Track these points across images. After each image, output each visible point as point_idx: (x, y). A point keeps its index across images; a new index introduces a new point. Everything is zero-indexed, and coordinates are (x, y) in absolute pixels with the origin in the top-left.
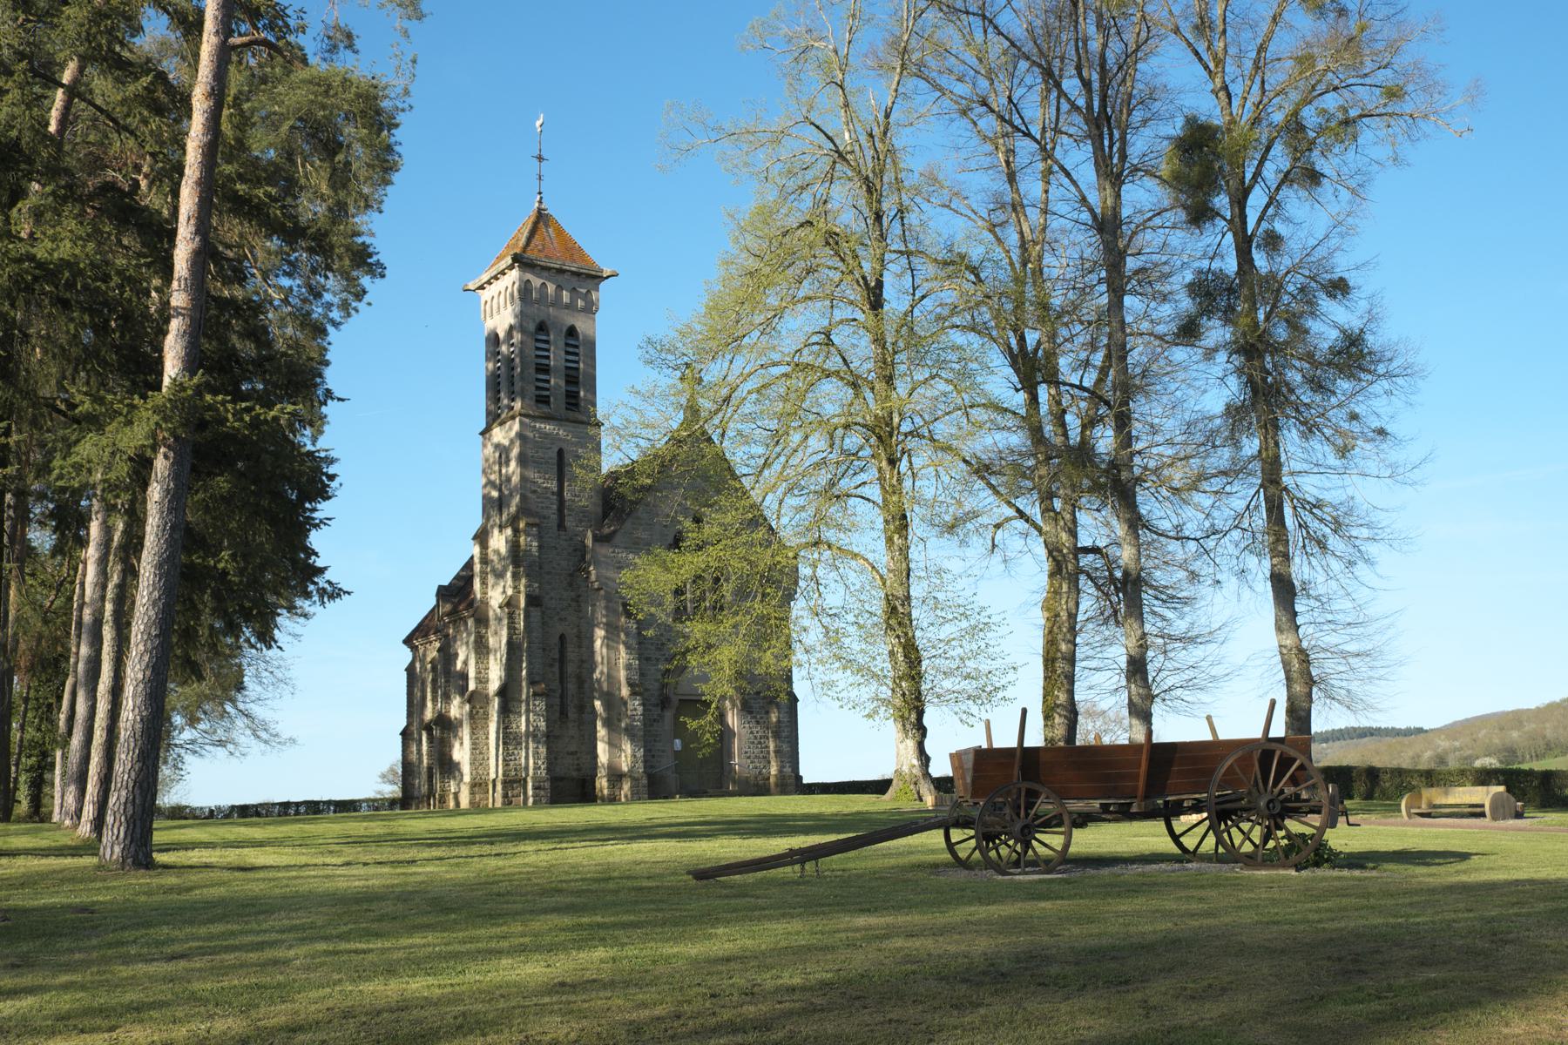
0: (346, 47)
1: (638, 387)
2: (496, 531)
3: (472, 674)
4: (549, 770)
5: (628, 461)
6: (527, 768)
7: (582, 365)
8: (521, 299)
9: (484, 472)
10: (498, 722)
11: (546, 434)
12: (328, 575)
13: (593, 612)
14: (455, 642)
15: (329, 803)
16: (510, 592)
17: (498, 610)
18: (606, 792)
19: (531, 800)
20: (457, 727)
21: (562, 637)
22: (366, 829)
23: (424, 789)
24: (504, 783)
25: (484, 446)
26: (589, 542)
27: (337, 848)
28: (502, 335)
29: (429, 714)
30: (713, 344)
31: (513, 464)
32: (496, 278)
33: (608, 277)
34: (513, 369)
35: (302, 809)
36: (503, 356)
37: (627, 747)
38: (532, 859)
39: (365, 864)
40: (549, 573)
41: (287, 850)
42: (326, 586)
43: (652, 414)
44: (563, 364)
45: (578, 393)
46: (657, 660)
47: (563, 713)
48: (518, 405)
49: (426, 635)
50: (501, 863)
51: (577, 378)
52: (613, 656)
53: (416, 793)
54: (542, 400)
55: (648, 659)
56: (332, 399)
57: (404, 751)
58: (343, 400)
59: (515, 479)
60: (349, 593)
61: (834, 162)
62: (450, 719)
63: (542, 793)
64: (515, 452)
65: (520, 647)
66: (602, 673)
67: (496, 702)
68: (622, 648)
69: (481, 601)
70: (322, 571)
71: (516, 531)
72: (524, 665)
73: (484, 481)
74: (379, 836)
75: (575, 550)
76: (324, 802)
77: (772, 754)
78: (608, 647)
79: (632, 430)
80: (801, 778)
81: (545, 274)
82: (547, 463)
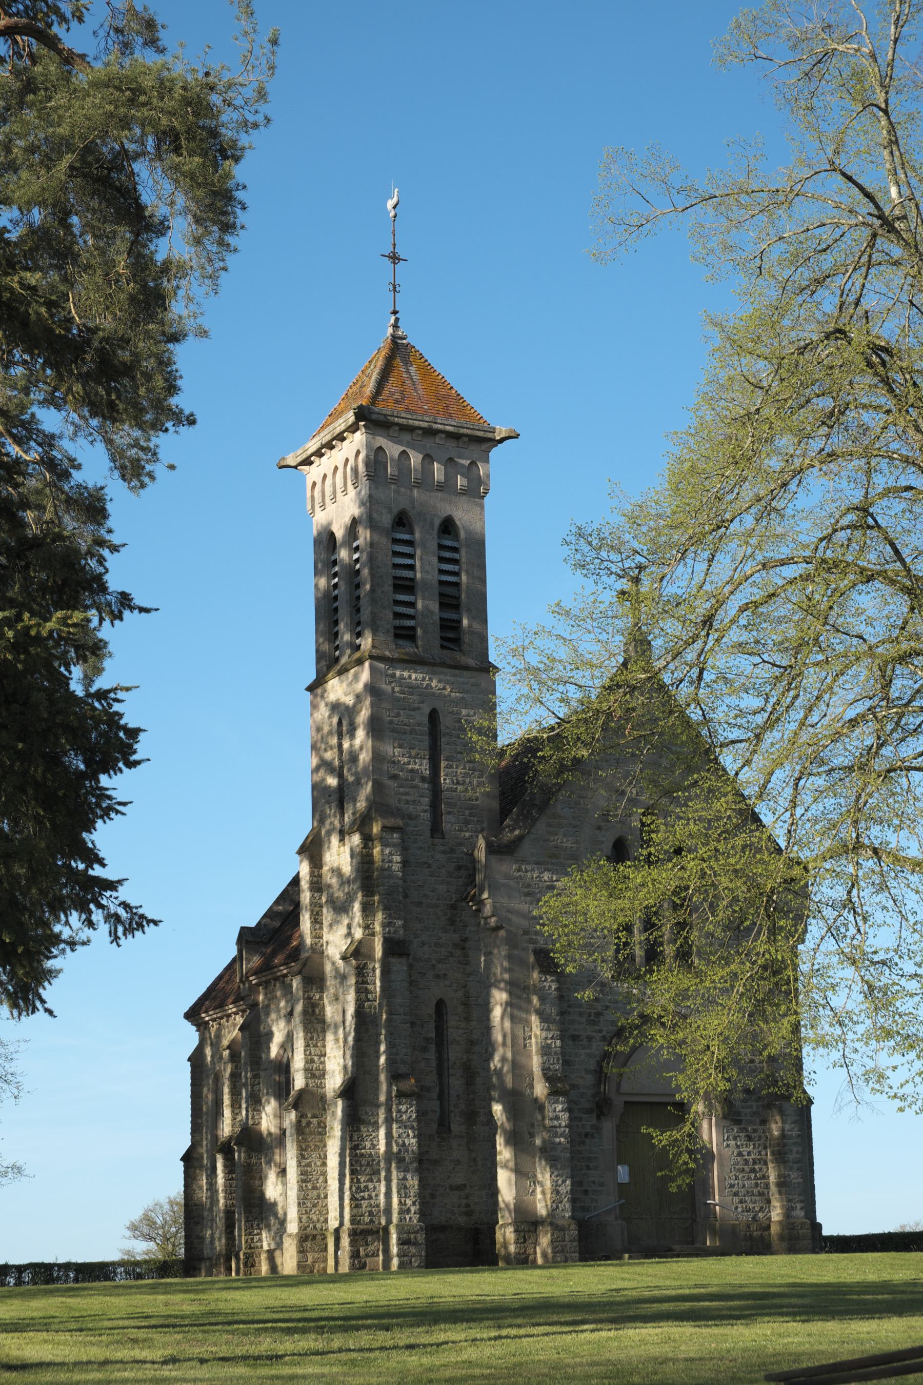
0: (145, 44)
1: (567, 604)
2: (335, 840)
3: (298, 1062)
4: (422, 1213)
5: (553, 721)
6: (388, 1211)
7: (464, 578)
8: (370, 477)
9: (314, 747)
10: (343, 1139)
11: (411, 687)
12: (123, 893)
13: (488, 963)
14: (268, 1014)
15: (67, 1266)
16: (358, 934)
17: (340, 963)
18: (512, 1248)
19: (395, 1262)
20: (270, 1148)
21: (440, 1006)
22: (166, 1304)
23: (220, 1245)
24: (353, 1234)
25: (314, 706)
26: (481, 854)
27: (141, 1334)
28: (339, 533)
29: (226, 1128)
30: (678, 536)
31: (360, 734)
32: (330, 446)
33: (502, 440)
34: (358, 586)
35: (27, 1277)
36: (343, 566)
37: (545, 1177)
38: (471, 1354)
39: (203, 1361)
40: (419, 904)
41: (62, 1337)
42: (121, 912)
43: (589, 646)
44: (434, 577)
45: (459, 621)
46: (590, 1039)
47: (444, 1125)
48: (366, 642)
49: (221, 1005)
50: (426, 1360)
51: (458, 598)
52: (520, 1033)
53: (207, 1252)
54: (404, 634)
55: (575, 1038)
56: (132, 608)
57: (187, 1185)
58: (147, 610)
59: (365, 757)
60: (156, 923)
61: (874, 236)
62: (260, 1134)
63: (413, 1250)
64: (364, 715)
65: (375, 1019)
66: (503, 1059)
67: (339, 1108)
68: (534, 1019)
69: (313, 948)
70: (112, 885)
71: (367, 839)
72: (383, 1048)
73: (315, 761)
74: (197, 1317)
75: (459, 868)
76: (60, 1266)
77: (773, 1189)
78: (513, 1018)
79: (559, 671)
80: (819, 1226)
81: (407, 437)
82: (412, 732)
